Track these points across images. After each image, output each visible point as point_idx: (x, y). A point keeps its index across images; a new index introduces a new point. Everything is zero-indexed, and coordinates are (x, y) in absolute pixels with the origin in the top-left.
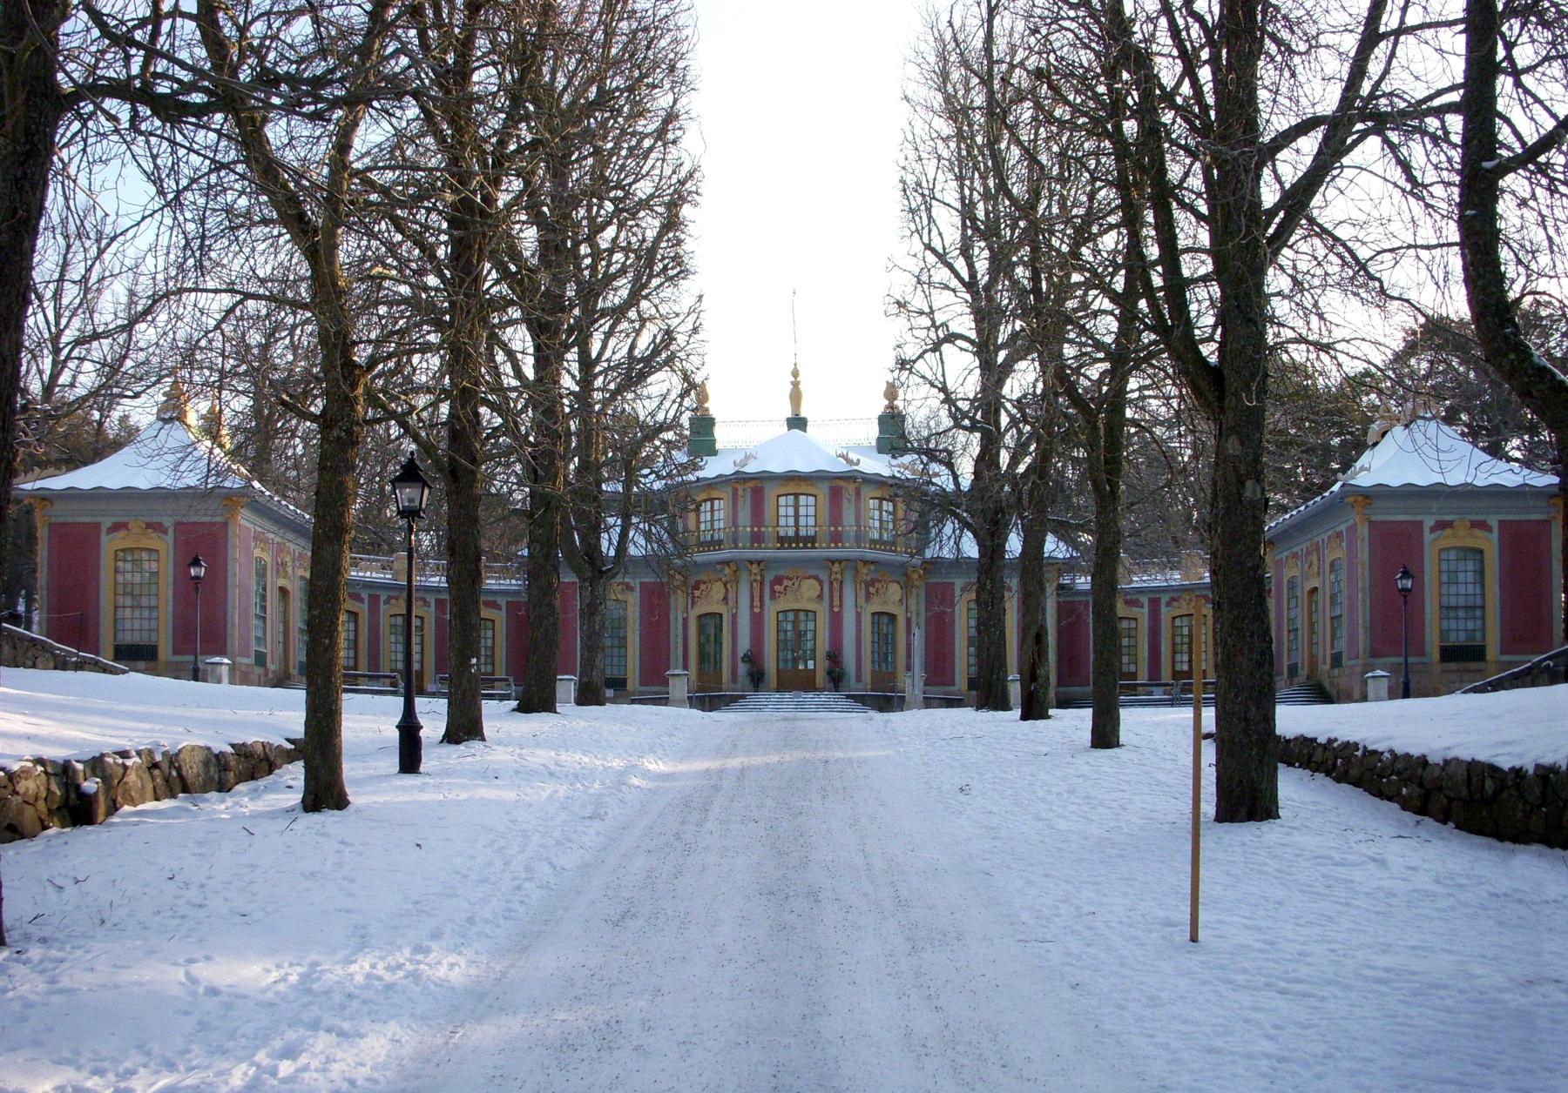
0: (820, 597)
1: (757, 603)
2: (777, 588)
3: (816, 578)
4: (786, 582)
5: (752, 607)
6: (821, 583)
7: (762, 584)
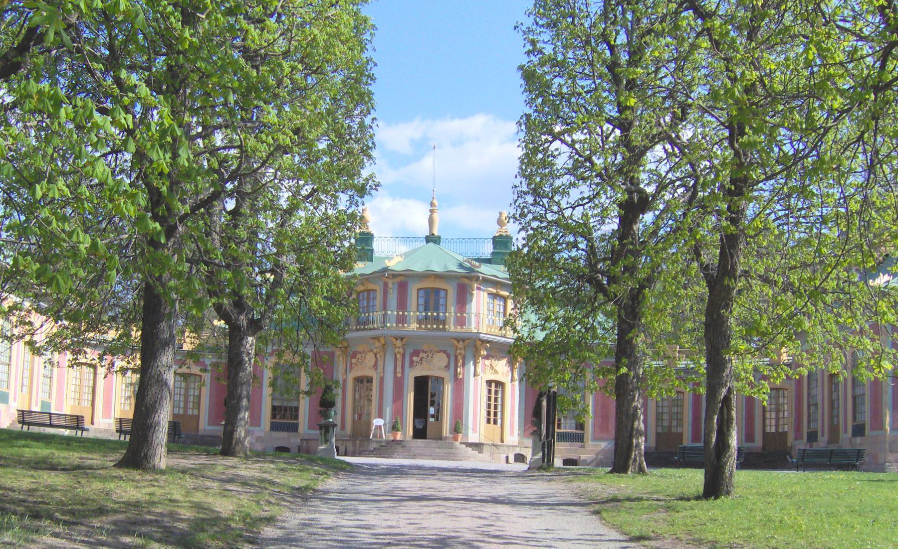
0: (447, 367)
1: (399, 369)
2: (415, 359)
3: (445, 352)
4: (421, 355)
5: (395, 373)
6: (448, 356)
7: (403, 356)
